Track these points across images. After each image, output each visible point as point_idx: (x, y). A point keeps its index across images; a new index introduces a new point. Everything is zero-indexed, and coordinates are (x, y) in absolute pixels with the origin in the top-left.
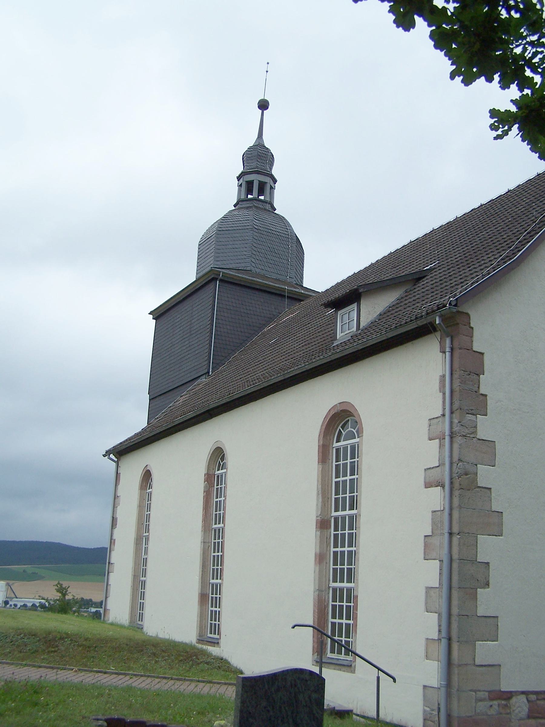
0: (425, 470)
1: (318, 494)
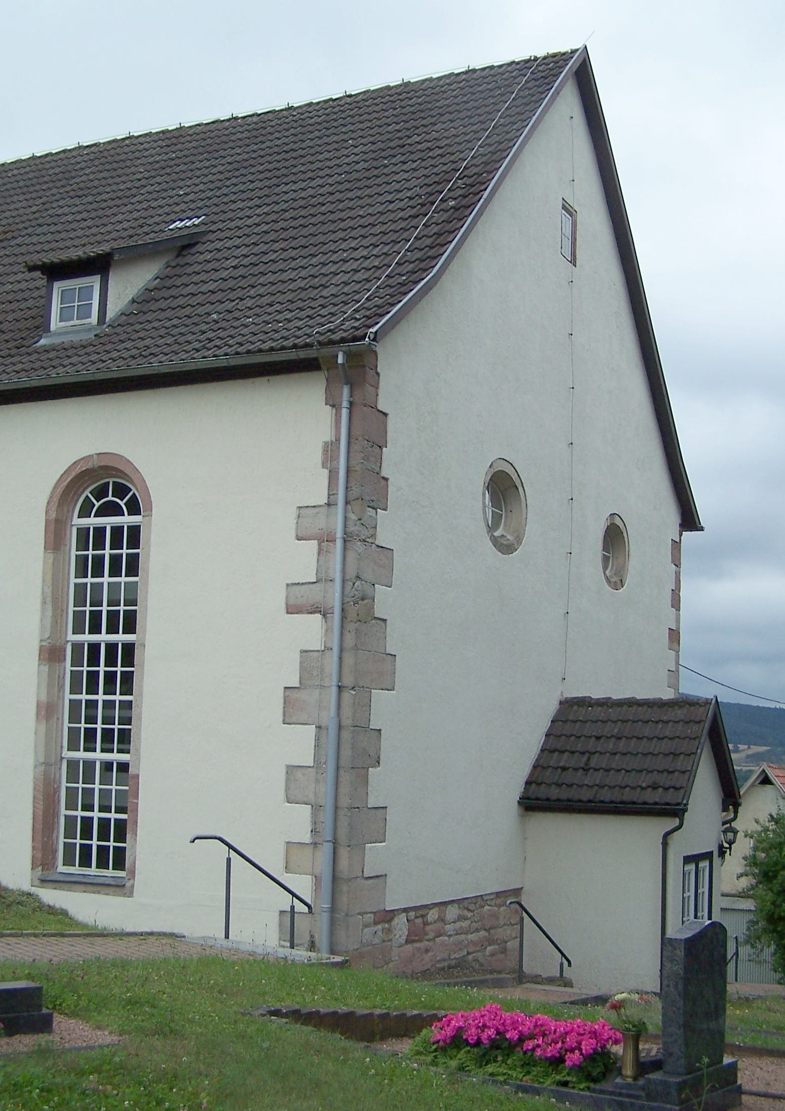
0: (288, 585)
1: (44, 602)
